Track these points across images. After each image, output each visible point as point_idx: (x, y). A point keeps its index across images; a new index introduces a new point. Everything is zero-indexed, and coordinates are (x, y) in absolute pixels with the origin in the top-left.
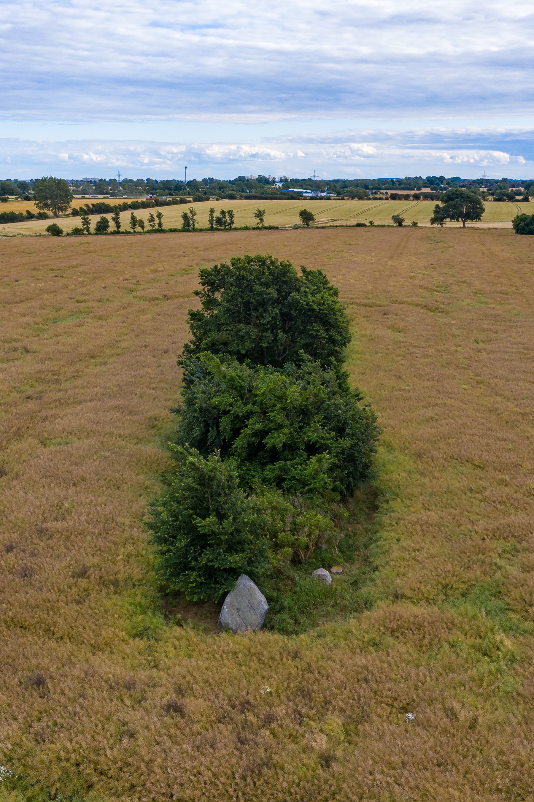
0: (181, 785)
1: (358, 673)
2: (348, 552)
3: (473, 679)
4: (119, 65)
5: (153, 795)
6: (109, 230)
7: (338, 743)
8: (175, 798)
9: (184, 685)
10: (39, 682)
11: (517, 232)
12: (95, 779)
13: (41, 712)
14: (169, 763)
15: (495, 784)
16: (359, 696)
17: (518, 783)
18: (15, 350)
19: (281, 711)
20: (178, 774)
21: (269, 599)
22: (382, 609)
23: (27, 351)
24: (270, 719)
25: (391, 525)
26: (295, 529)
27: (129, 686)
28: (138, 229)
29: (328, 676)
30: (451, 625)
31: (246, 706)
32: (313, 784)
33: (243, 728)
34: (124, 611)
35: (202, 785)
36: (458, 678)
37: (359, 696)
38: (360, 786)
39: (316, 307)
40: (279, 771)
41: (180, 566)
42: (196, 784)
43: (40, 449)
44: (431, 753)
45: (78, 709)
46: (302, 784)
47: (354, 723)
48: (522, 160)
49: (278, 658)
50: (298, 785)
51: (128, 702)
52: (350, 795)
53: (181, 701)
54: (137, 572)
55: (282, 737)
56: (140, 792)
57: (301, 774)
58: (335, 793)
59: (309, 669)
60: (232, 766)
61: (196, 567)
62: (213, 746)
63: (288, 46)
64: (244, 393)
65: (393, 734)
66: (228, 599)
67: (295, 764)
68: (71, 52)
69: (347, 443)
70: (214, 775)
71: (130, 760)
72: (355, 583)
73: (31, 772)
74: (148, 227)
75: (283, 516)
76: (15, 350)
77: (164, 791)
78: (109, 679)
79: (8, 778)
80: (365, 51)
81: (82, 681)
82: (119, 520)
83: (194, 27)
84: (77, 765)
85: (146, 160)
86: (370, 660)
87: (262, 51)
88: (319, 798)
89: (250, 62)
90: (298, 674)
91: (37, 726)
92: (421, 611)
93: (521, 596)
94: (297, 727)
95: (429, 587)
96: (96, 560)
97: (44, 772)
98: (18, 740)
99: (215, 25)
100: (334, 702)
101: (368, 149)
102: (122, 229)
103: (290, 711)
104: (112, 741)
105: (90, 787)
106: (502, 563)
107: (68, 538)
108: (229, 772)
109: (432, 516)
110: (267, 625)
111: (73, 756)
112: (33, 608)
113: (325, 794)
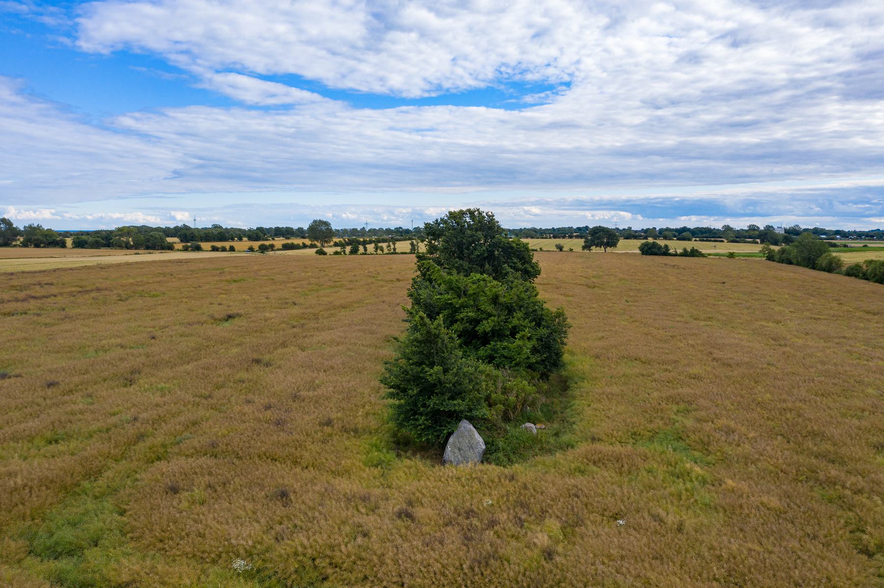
0: (412, 575)
1: (568, 490)
2: (550, 415)
3: (672, 494)
4: (367, 155)
5: (385, 583)
6: (359, 252)
7: (558, 542)
8: (405, 586)
9: (413, 498)
10: (284, 495)
11: (643, 254)
12: (330, 571)
13: (282, 518)
14: (400, 556)
15: (712, 574)
16: (573, 507)
17: (733, 573)
18: (287, 303)
19: (503, 517)
20: (409, 566)
21: (486, 443)
22: (583, 447)
23: (295, 304)
24: (492, 523)
25: (581, 396)
26: (505, 391)
27: (365, 499)
28: (379, 252)
29: (542, 493)
30: (645, 458)
31: (470, 513)
32: (539, 574)
33: (469, 530)
34: (361, 448)
35: (432, 575)
36: (659, 493)
37: (573, 507)
38: (583, 575)
39: (514, 245)
40: (506, 563)
41: (408, 414)
42: (426, 575)
43: (299, 352)
44: (646, 549)
45: (317, 514)
46: (527, 573)
47: (571, 527)
48: (640, 217)
49: (496, 480)
50: (524, 575)
51: (363, 510)
52: (575, 582)
53: (410, 509)
54: (373, 423)
55: (505, 537)
56: (373, 582)
57: (526, 565)
58: (560, 582)
59: (525, 487)
60: (460, 558)
61: (424, 415)
62: (441, 542)
63: (481, 143)
64: (460, 292)
65: (607, 534)
66: (451, 440)
67: (518, 556)
68: (335, 146)
69: (544, 332)
70: (443, 567)
71: (363, 554)
72: (557, 434)
73: (269, 565)
74: (386, 251)
75: (495, 381)
76: (287, 303)
77: (395, 579)
78: (346, 493)
79: (246, 571)
80: (532, 146)
81: (322, 495)
82: (360, 390)
83: (418, 130)
84: (314, 560)
85: (385, 218)
86: (579, 480)
87: (463, 146)
88: (546, 586)
89: (455, 153)
90: (515, 492)
91: (278, 528)
92: (618, 448)
93: (701, 439)
94: (519, 529)
95: (620, 433)
96: (339, 415)
97: (281, 566)
98: (259, 538)
99: (431, 129)
100: (550, 511)
101: (535, 210)
102: (368, 252)
103: (511, 517)
104: (346, 540)
105: (325, 579)
106: (680, 418)
107: (317, 402)
108: (457, 564)
109: (615, 389)
110: (486, 457)
111: (309, 551)
112: (283, 446)
113: (551, 582)
